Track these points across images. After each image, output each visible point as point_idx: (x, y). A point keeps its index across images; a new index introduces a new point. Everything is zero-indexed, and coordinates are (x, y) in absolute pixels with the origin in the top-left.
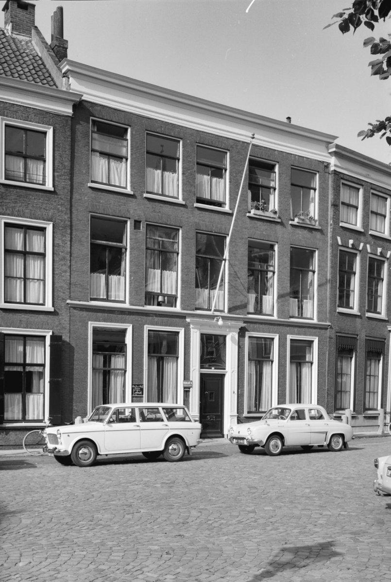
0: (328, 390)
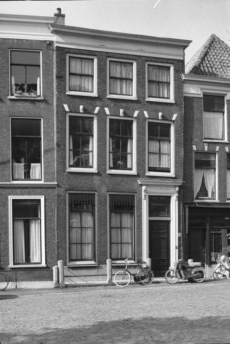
0: (57, 243)
